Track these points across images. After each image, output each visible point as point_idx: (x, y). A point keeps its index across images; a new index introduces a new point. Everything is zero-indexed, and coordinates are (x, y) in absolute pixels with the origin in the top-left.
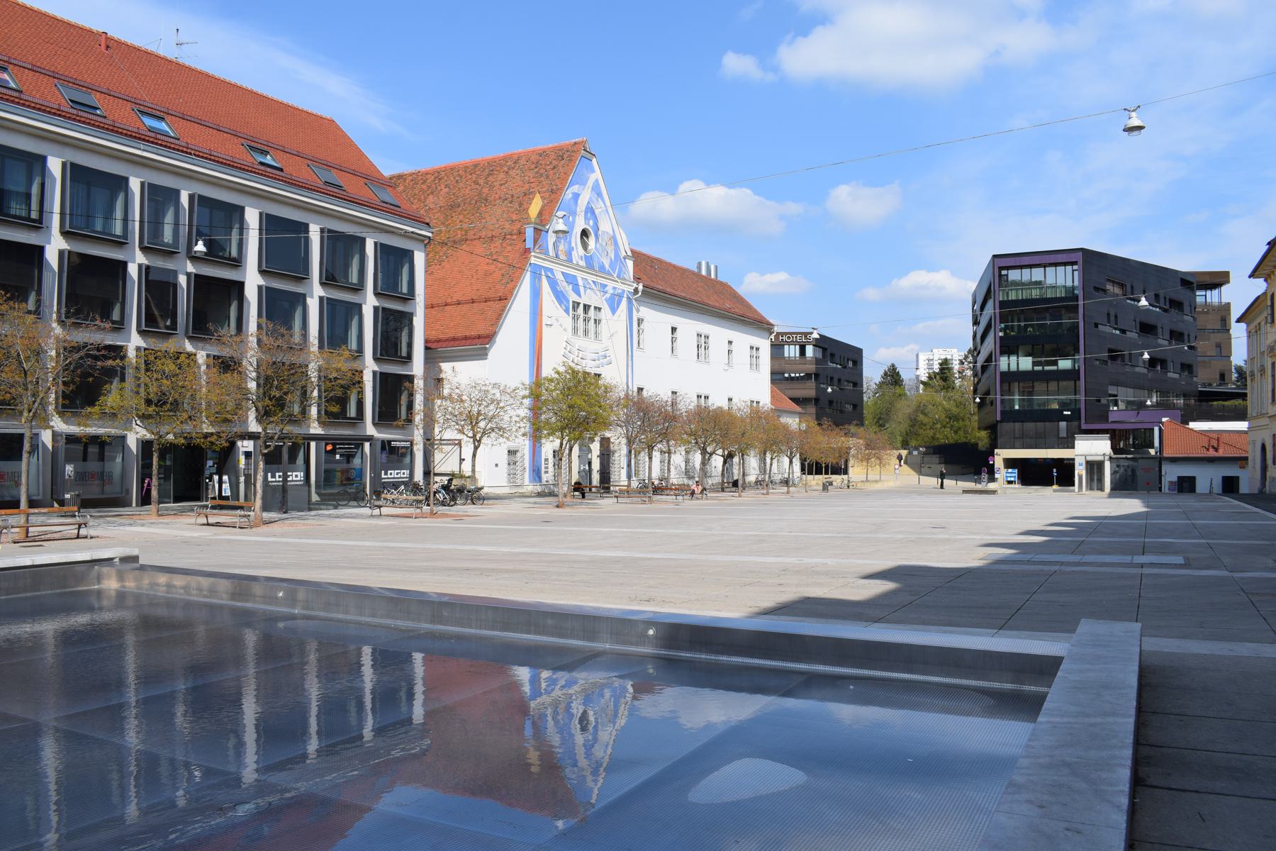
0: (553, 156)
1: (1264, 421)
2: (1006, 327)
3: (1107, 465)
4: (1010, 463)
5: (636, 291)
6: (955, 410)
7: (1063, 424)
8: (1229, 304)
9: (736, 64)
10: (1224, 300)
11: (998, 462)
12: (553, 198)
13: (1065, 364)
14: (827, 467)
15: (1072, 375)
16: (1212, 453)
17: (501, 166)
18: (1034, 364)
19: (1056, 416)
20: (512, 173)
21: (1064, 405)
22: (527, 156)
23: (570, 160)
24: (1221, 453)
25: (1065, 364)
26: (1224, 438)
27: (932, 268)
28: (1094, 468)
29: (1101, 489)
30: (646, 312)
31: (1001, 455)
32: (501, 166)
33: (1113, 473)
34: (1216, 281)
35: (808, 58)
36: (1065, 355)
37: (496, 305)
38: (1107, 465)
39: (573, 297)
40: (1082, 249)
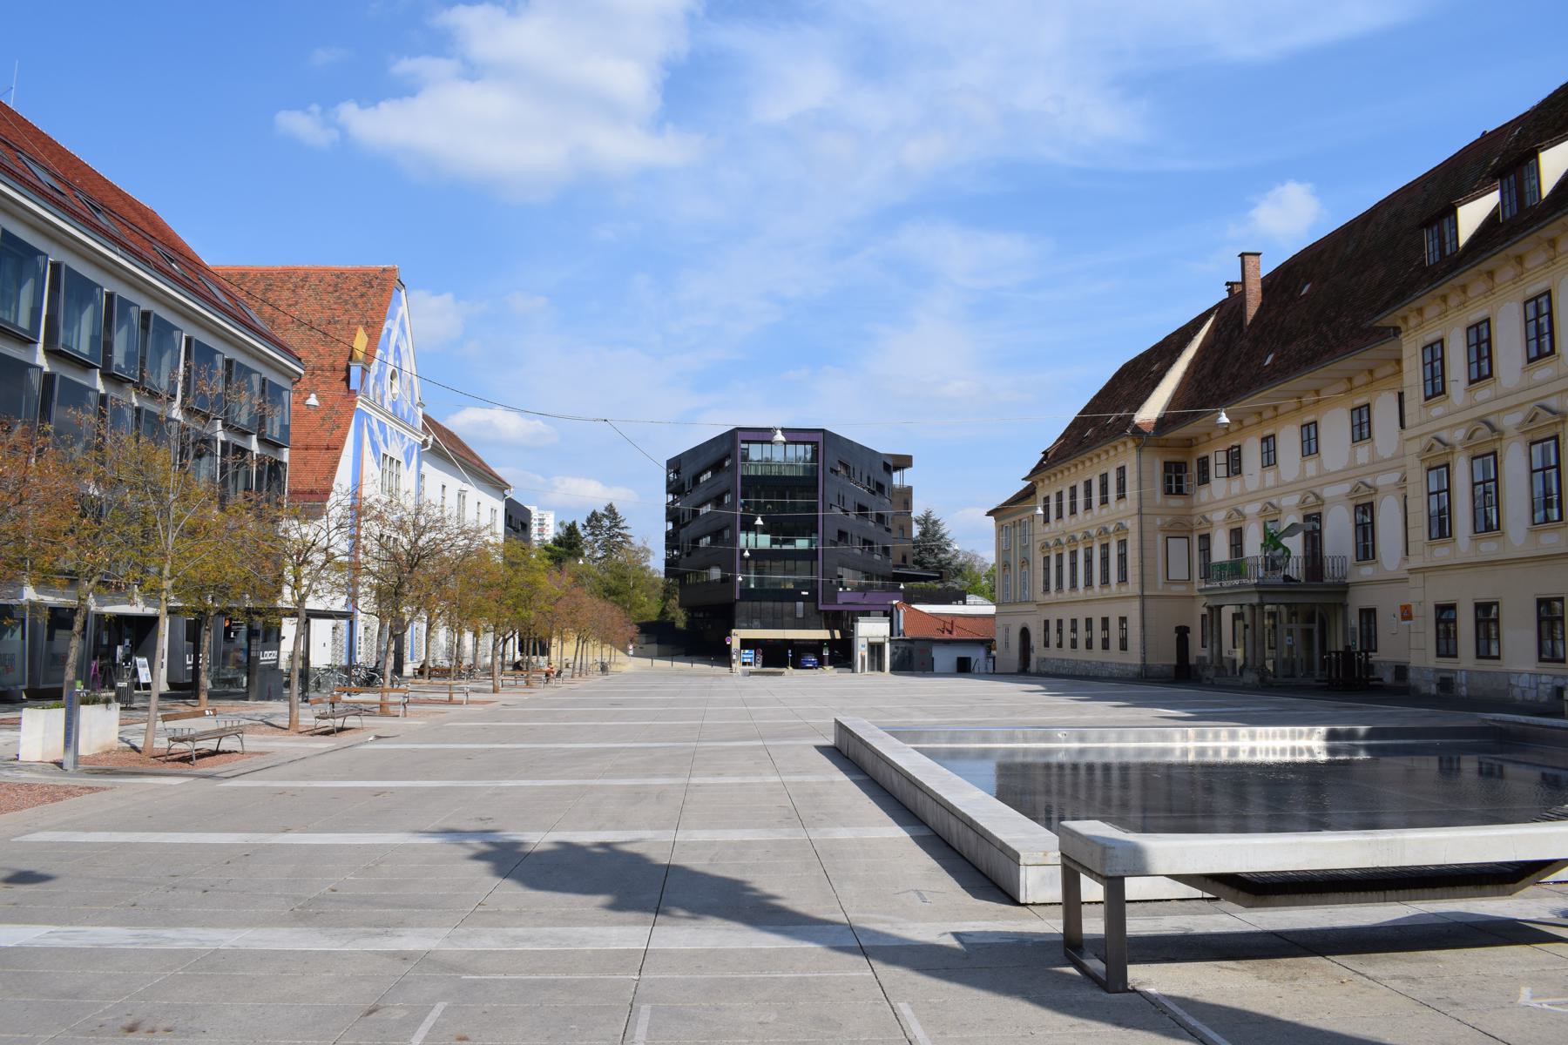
0: (356, 281)
1: (1032, 607)
2: (746, 503)
3: (887, 646)
4: (745, 644)
5: (425, 443)
6: (614, 583)
7: (800, 604)
8: (910, 489)
9: (300, 124)
10: (906, 484)
11: (735, 643)
12: (374, 330)
13: (802, 544)
14: (1448, 621)
15: (810, 555)
16: (947, 636)
17: (284, 282)
18: (773, 542)
19: (793, 596)
20: (303, 293)
21: (800, 585)
22: (321, 275)
23: (384, 290)
24: (955, 636)
25: (802, 544)
26: (957, 622)
27: (488, 403)
28: (876, 649)
29: (881, 668)
30: (427, 468)
31: (737, 636)
32: (284, 282)
33: (892, 654)
34: (899, 463)
35: (379, 126)
36: (802, 535)
37: (332, 453)
38: (887, 646)
39: (383, 450)
40: (823, 430)
